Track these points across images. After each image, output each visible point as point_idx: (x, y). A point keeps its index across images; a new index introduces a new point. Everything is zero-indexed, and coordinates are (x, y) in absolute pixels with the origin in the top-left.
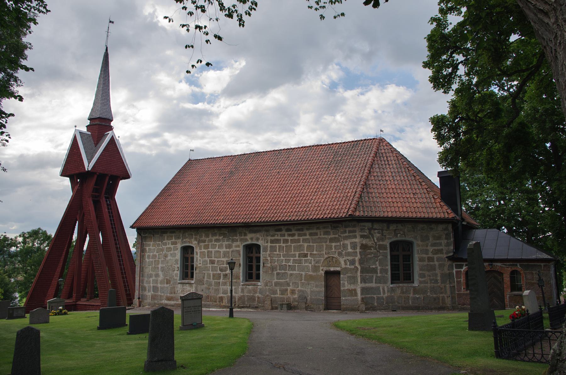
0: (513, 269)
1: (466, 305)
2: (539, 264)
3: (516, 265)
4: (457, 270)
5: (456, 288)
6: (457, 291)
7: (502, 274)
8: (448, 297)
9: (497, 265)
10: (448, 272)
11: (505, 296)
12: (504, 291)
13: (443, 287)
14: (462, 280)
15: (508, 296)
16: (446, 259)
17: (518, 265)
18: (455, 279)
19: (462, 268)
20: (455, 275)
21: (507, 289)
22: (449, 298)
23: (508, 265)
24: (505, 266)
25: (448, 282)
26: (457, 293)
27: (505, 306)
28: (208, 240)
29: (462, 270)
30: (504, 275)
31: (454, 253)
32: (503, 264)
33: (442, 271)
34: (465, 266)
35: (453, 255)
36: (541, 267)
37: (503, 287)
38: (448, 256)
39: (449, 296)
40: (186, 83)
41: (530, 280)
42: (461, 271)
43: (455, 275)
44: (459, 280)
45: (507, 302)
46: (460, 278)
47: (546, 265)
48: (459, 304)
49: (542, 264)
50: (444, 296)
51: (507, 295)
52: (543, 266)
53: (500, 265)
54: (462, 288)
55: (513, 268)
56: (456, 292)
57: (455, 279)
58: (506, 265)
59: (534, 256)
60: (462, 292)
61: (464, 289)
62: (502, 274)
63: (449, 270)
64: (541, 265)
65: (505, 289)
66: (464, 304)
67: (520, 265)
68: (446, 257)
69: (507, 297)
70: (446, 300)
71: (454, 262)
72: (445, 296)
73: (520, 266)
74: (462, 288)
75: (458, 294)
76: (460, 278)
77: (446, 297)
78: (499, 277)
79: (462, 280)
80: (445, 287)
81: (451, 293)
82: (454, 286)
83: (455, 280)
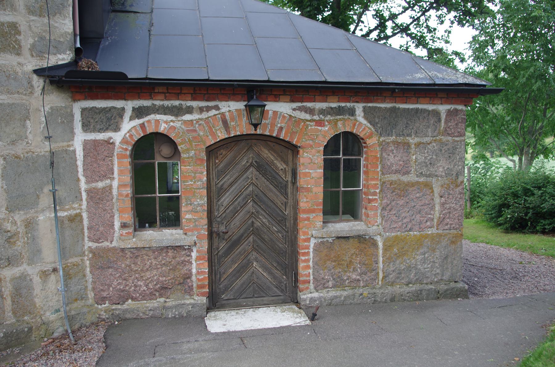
0: (341, 128)
1: (133, 299)
2: (430, 107)
3: (352, 112)
4: (92, 136)
5: (86, 222)
6: (90, 239)
7: (294, 149)
8: (44, 275)
9: (275, 113)
10: (46, 147)
11: (301, 243)
12: (295, 223)
13: (22, 230)
14: (115, 184)
15: (313, 242)
16: (38, 83)
17: (359, 108)
18: (83, 179)
19: (117, 129)
20: (80, 163)
21: (311, 216)
22: (53, 277)
23: (322, 112)
24: (308, 117)
25: (46, 200)
26: (91, 250)
27: (296, 287)
28: (492, 157)
29: (117, 137)
30: (305, 157)
31: (78, 51)
32: (300, 109)
33: (13, 143)
34: (131, 119)
35: (75, 62)
36: (440, 120)
37: (296, 204)
38: (44, 64)
39: (50, 267)
40: (75, 102)
41: (397, 172)
42: (109, 143)
43: (80, 163)
44: (100, 185)
45: (308, 267)
46: (108, 174)
47: (394, 109)
48: (101, 300)
49: (443, 108)
50: (23, 277)
51: (308, 240)
52: (443, 116)
53: (290, 112)
54: (117, 224)
55: (340, 124)
56: (88, 244)
57: (83, 179)
58: (311, 111)
59: (418, 75)
60: (114, 244)
61: (124, 226)
62: (294, 149)
63: (49, 138)
64: (436, 114)
65: (302, 216)
66: (124, 297)
67: (365, 109)
68: (36, 72)
69: (308, 247)
70: (37, 290)
71: (75, 100)
72: (33, 271)
73: (365, 117)
74: (117, 224)
75: (96, 254)
76: (104, 177)
77: (37, 280)
78: (280, 165)
79: (115, 184)
80: (30, 225)
81: (63, 252)
82: (76, 219)
83: (83, 185)
